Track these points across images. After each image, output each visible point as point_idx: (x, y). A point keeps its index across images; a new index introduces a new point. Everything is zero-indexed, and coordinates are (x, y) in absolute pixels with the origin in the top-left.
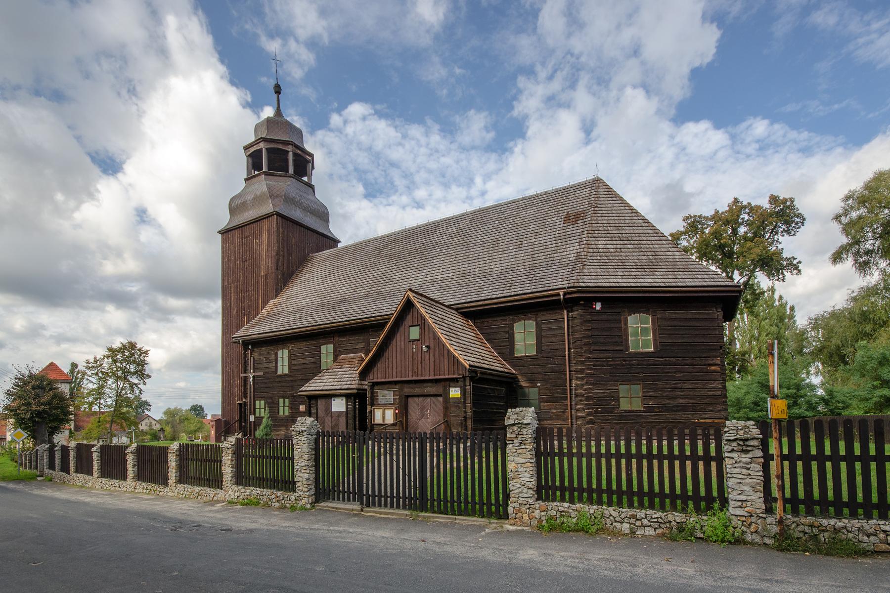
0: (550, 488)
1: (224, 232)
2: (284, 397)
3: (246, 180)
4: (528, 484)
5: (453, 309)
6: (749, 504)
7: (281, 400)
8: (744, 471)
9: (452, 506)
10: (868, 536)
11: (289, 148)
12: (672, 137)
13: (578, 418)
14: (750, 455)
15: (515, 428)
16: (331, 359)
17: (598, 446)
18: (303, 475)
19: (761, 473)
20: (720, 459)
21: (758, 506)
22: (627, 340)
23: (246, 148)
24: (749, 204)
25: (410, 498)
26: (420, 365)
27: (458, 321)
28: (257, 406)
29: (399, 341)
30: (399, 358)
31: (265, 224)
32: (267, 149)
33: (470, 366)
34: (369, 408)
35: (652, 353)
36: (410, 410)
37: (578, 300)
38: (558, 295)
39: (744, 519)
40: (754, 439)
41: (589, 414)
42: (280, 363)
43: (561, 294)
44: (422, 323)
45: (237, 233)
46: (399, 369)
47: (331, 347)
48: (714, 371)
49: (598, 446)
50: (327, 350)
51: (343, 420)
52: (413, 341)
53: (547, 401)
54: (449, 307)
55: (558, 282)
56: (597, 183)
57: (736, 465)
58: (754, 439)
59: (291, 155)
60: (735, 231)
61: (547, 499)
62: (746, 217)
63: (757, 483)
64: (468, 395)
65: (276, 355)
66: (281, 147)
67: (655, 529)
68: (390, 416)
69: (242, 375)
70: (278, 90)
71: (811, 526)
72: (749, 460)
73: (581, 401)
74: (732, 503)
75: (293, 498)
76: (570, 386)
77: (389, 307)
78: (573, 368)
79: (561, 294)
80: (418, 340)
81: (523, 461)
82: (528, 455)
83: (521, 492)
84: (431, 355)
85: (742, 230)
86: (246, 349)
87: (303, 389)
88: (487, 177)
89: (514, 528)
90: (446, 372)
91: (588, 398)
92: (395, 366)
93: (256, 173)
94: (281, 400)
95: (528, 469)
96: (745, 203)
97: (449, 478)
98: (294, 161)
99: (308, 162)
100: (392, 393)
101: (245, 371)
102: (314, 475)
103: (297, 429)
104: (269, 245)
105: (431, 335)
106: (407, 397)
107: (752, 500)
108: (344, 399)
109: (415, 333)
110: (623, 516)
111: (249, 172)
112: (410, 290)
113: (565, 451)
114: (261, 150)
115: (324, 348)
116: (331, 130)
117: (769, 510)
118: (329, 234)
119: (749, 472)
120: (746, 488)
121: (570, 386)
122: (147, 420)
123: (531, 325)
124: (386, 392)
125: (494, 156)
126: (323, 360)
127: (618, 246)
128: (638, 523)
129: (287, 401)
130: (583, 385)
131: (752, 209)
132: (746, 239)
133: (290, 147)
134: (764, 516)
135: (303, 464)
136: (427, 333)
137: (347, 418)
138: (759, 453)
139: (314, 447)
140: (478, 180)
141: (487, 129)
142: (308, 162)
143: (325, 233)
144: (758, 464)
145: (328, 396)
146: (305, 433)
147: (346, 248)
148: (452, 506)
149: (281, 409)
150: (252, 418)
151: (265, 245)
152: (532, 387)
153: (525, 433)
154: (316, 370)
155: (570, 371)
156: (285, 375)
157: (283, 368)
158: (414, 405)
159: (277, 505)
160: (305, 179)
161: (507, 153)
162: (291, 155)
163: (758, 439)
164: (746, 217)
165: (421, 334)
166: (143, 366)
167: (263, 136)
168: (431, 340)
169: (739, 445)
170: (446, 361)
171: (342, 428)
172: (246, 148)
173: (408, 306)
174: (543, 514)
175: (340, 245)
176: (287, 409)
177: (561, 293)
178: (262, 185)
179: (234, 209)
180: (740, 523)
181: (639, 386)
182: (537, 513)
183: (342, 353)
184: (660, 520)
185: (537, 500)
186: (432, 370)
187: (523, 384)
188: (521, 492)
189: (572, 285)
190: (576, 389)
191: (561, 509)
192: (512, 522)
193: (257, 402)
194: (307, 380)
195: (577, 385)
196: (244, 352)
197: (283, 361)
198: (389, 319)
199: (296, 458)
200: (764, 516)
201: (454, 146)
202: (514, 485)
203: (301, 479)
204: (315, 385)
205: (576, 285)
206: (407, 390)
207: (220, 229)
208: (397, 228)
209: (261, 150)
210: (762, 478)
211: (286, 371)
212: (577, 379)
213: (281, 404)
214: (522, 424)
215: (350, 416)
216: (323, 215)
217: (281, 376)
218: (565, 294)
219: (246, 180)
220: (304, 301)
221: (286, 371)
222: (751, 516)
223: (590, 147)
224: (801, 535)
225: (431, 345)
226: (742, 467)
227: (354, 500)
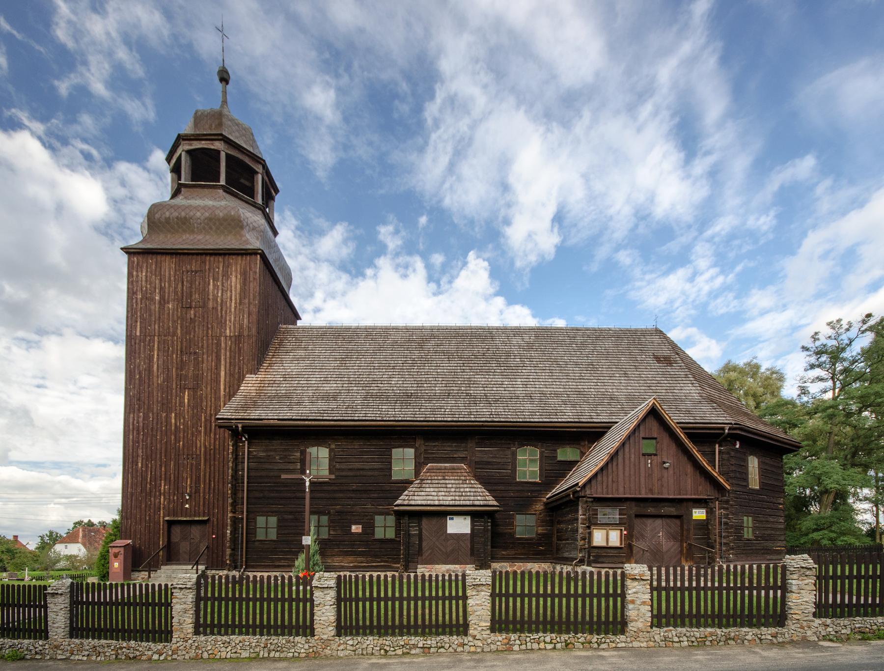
0: (150, 604)
2: (267, 514)
7: (745, 518)
12: (501, 312)
17: (851, 570)
30: (627, 474)
31: (237, 265)
35: (757, 490)
38: (723, 429)
45: (168, 265)
47: (410, 452)
49: (851, 570)
66: (247, 160)
87: (398, 502)
88: (332, 295)
94: (377, 518)
97: (679, 604)
100: (617, 512)
104: (244, 292)
116: (145, 169)
124: (608, 510)
125: (345, 277)
133: (261, 167)
140: (319, 295)
141: (345, 241)
145: (442, 514)
147: (304, 329)
159: (48, 657)
161: (360, 278)
177: (727, 427)
201: (306, 251)
208: (475, 322)
218: (730, 429)
223: (436, 299)
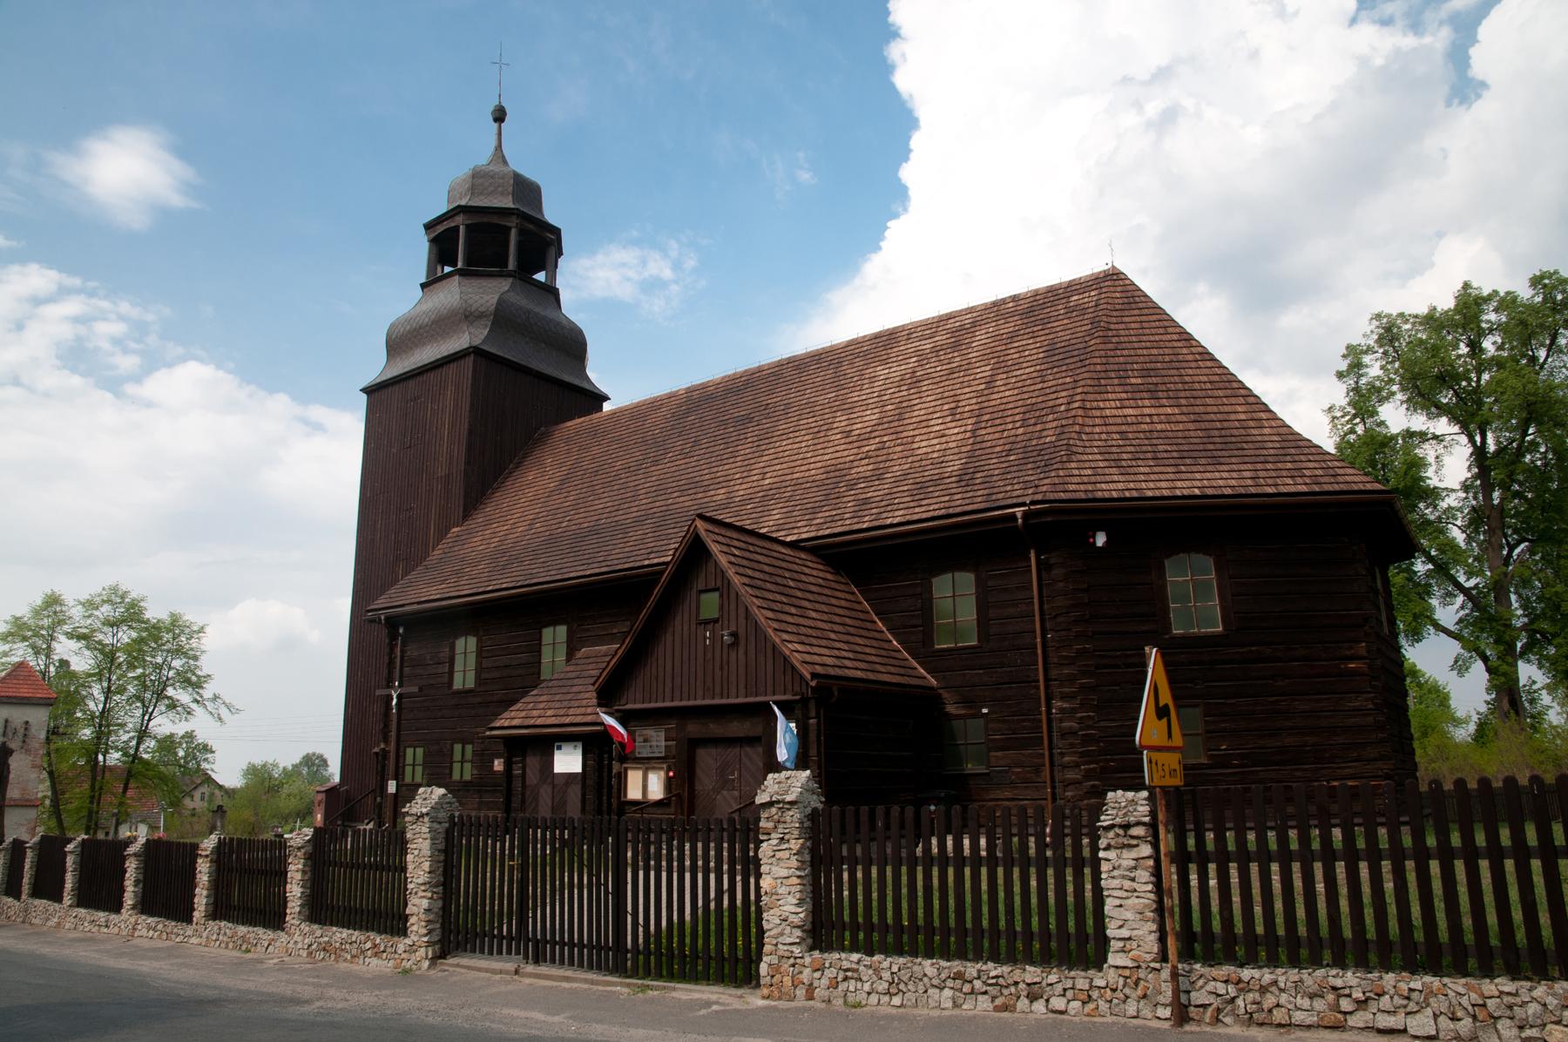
1: (370, 391)
3: (423, 286)
4: (793, 918)
5: (804, 549)
6: (1134, 944)
8: (1127, 884)
9: (647, 962)
10: (1312, 997)
11: (513, 222)
13: (1068, 784)
14: (1134, 854)
15: (774, 810)
16: (561, 657)
18: (419, 904)
19: (1150, 887)
20: (1096, 863)
21: (1147, 948)
22: (1166, 610)
23: (429, 227)
24: (1496, 292)
25: (599, 948)
26: (718, 672)
27: (815, 572)
28: (409, 760)
29: (681, 624)
32: (467, 226)
33: (814, 676)
34: (616, 767)
36: (698, 771)
37: (1059, 526)
39: (1127, 973)
40: (1138, 824)
41: (1088, 775)
42: (458, 666)
43: (1019, 515)
44: (723, 587)
46: (678, 681)
48: (1354, 672)
50: (555, 637)
51: (574, 795)
52: (706, 622)
53: (1005, 746)
54: (793, 545)
55: (1018, 492)
56: (1112, 279)
57: (1116, 873)
58: (1138, 824)
59: (513, 233)
60: (1475, 347)
61: (828, 948)
62: (1493, 317)
63: (1146, 906)
64: (813, 736)
65: (453, 648)
66: (495, 220)
67: (994, 998)
68: (656, 787)
69: (379, 692)
70: (500, 116)
71: (1226, 982)
72: (1132, 863)
73: (1072, 745)
74: (1115, 945)
75: (401, 948)
76: (1049, 712)
77: (664, 552)
78: (1054, 673)
79: (1019, 515)
80: (716, 621)
81: (784, 873)
82: (794, 863)
83: (782, 934)
84: (741, 652)
85: (1489, 344)
86: (393, 636)
89: (765, 1002)
90: (770, 689)
91: (1086, 740)
92: (672, 678)
93: (447, 269)
94: (458, 747)
95: (793, 889)
96: (1485, 292)
98: (520, 245)
99: (548, 244)
100: (662, 734)
101: (389, 685)
102: (440, 903)
103: (414, 811)
105: (742, 611)
106: (694, 743)
107: (1140, 938)
108: (580, 745)
109: (710, 604)
110: (943, 976)
111: (431, 269)
112: (701, 516)
113: (984, 853)
114: (456, 229)
115: (547, 633)
117: (1164, 958)
118: (587, 386)
119: (1135, 885)
120: (1129, 915)
121: (1049, 712)
122: (205, 789)
123: (966, 580)
124: (650, 732)
126: (546, 658)
127: (1147, 411)
128: (967, 988)
129: (469, 748)
130: (1074, 711)
131: (1507, 302)
132: (1498, 363)
134: (1157, 965)
135: (420, 881)
136: (733, 606)
137: (584, 786)
138: (1146, 850)
139: (442, 846)
142: (548, 244)
143: (576, 382)
144: (1146, 869)
146: (426, 819)
148: (647, 962)
149: (457, 767)
150: (392, 787)
151: (450, 412)
152: (973, 716)
153: (788, 819)
154: (525, 679)
155: (1047, 680)
156: (470, 691)
157: (464, 676)
158: (707, 759)
160: (541, 276)
162: (513, 233)
163: (1144, 824)
164: (1493, 317)
165: (721, 608)
166: (196, 658)
167: (463, 203)
168: (742, 621)
169: (1118, 835)
170: (770, 662)
171: (573, 810)
172: (429, 227)
173: (694, 554)
174: (817, 975)
175: (607, 407)
176: (468, 766)
177: (1019, 511)
178: (452, 294)
179: (397, 344)
180: (1121, 981)
181: (1197, 711)
182: (806, 975)
183: (585, 642)
184: (1001, 981)
185: (811, 949)
186: (742, 686)
187: (951, 709)
188: (782, 934)
189: (1039, 497)
190: (1061, 720)
191: (846, 965)
192: (765, 991)
193: (410, 751)
194: (508, 703)
195: (1062, 710)
196: (389, 643)
197: (465, 661)
198: (662, 572)
199: (410, 867)
200: (1157, 965)
202: (771, 920)
203: (415, 910)
204: (513, 719)
205: (1051, 496)
206: (694, 729)
207: (365, 383)
209: (456, 229)
210: (1152, 896)
211: (470, 684)
212: (1063, 697)
213: (457, 756)
214: (783, 801)
215: (590, 782)
216: (573, 345)
217: (459, 692)
219: (423, 286)
220: (530, 530)
221: (470, 684)
222: (1138, 967)
224: (1211, 999)
225: (742, 632)
226: (1124, 877)
227: (509, 952)
